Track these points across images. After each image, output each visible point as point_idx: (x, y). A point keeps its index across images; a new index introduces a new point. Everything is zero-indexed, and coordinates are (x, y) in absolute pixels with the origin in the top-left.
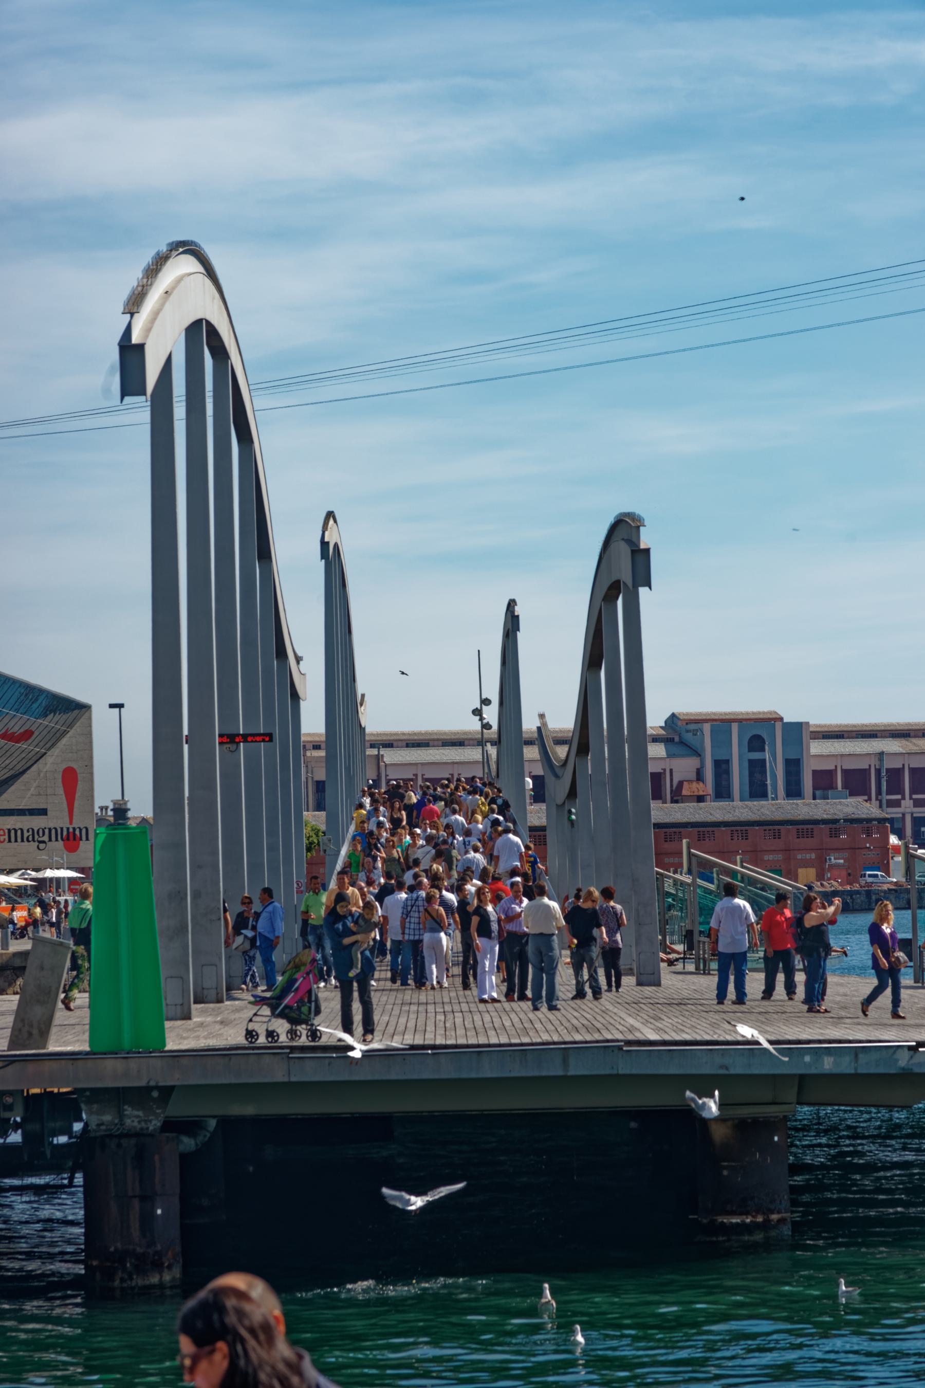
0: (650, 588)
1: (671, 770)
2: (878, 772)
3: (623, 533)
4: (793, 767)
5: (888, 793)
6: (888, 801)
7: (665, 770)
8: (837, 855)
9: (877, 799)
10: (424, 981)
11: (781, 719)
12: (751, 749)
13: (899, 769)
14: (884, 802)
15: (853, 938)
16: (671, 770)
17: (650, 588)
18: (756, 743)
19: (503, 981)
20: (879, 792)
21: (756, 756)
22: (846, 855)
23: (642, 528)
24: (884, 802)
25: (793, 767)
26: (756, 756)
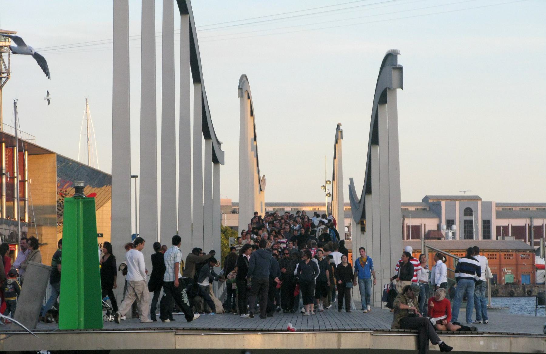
0: (402, 89)
1: (425, 225)
2: (530, 227)
3: (390, 60)
4: (487, 224)
5: (534, 239)
6: (534, 242)
7: (421, 224)
8: (508, 268)
9: (529, 241)
10: (254, 302)
11: (481, 199)
12: (465, 214)
13: (523, 226)
14: (533, 243)
15: (515, 260)
16: (425, 225)
17: (402, 89)
18: (468, 212)
19: (5, 39)
20: (530, 238)
21: (468, 218)
22: (513, 268)
23: (398, 55)
24: (533, 243)
25: (487, 224)
26: (468, 218)
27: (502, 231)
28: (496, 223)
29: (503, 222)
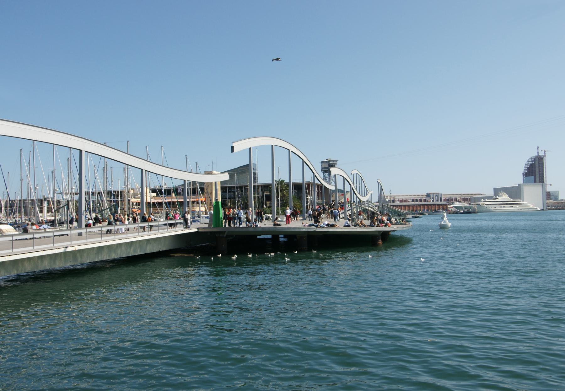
25: (441, 199)
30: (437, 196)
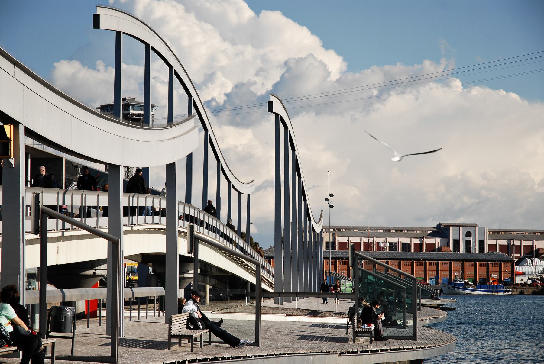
25: (482, 243)
27: (492, 248)
28: (489, 242)
29: (493, 242)
30: (468, 234)
